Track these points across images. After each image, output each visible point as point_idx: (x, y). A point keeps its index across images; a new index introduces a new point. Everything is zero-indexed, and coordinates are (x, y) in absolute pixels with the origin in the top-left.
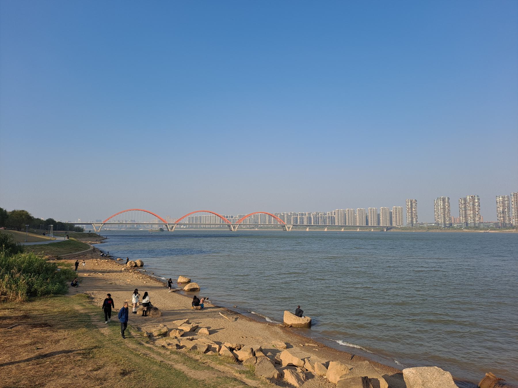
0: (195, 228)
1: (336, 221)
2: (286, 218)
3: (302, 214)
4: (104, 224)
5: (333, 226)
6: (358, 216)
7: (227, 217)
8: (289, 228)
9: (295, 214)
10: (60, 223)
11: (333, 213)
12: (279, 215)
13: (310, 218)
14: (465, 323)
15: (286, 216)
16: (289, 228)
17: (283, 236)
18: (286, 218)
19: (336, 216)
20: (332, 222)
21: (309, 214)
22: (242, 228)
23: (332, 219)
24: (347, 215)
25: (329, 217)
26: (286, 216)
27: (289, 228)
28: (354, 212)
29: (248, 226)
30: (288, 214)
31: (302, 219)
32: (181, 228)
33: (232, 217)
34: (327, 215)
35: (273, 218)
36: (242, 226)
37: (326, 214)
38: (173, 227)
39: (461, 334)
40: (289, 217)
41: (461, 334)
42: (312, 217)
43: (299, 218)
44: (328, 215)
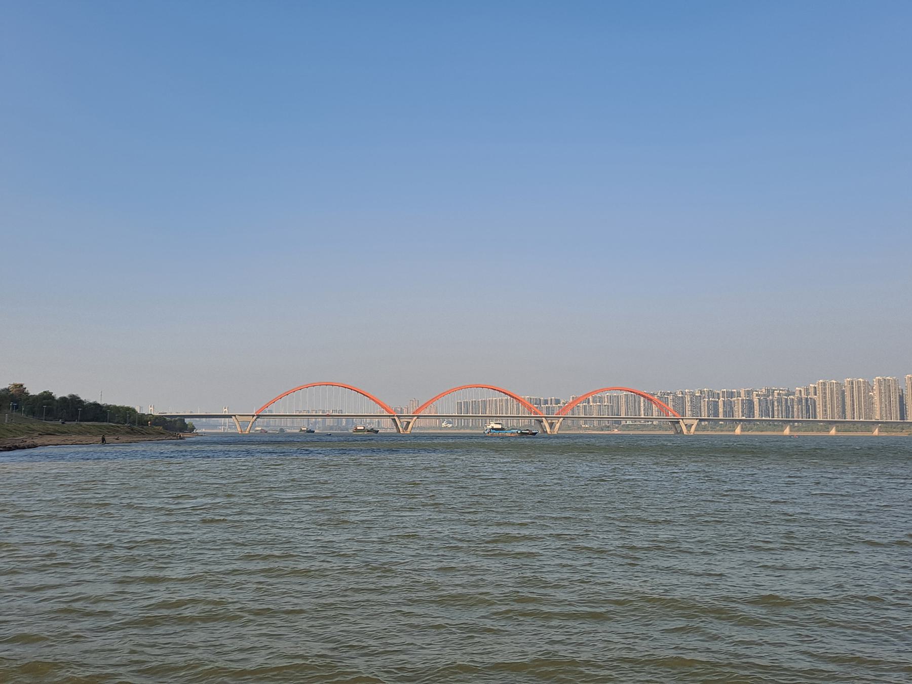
0: (471, 428)
1: (819, 410)
2: (688, 404)
3: (731, 395)
4: (258, 416)
5: (812, 424)
6: (876, 398)
7: (546, 402)
8: (690, 426)
9: (712, 394)
10: (96, 406)
11: (811, 391)
12: (671, 397)
13: (751, 402)
14: (187, 613)
15: (688, 398)
16: (689, 427)
17: (673, 448)
18: (688, 404)
19: (818, 399)
20: (808, 411)
21: (749, 393)
22: (580, 428)
23: (809, 406)
24: (847, 394)
25: (800, 401)
26: (688, 398)
27: (689, 427)
28: (868, 387)
29: (596, 423)
30: (675, 395)
31: (729, 407)
32: (441, 428)
33: (558, 402)
34: (798, 395)
35: (642, 399)
36: (582, 422)
37: (794, 394)
38: (409, 423)
39: (328, 660)
40: (696, 402)
41: (328, 660)
42: (756, 400)
43: (721, 404)
44: (798, 395)
